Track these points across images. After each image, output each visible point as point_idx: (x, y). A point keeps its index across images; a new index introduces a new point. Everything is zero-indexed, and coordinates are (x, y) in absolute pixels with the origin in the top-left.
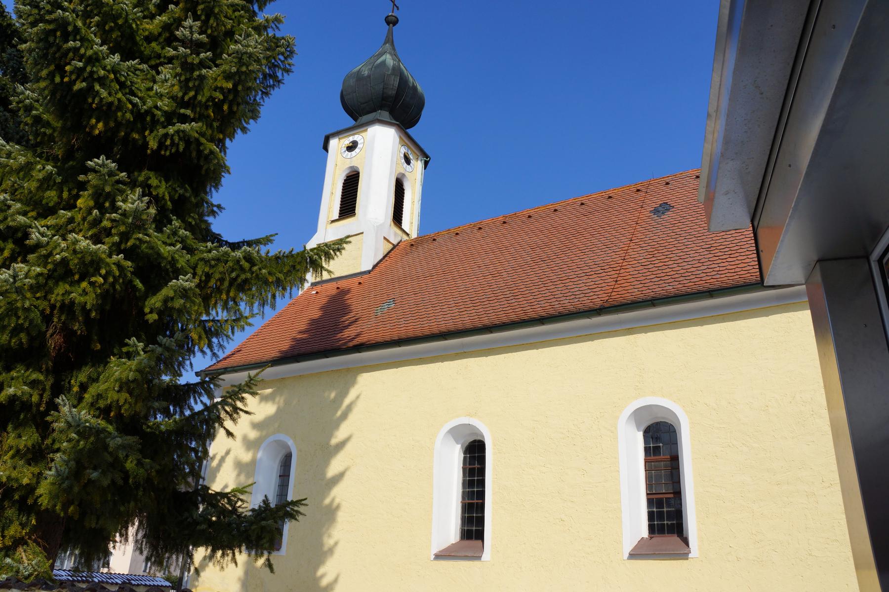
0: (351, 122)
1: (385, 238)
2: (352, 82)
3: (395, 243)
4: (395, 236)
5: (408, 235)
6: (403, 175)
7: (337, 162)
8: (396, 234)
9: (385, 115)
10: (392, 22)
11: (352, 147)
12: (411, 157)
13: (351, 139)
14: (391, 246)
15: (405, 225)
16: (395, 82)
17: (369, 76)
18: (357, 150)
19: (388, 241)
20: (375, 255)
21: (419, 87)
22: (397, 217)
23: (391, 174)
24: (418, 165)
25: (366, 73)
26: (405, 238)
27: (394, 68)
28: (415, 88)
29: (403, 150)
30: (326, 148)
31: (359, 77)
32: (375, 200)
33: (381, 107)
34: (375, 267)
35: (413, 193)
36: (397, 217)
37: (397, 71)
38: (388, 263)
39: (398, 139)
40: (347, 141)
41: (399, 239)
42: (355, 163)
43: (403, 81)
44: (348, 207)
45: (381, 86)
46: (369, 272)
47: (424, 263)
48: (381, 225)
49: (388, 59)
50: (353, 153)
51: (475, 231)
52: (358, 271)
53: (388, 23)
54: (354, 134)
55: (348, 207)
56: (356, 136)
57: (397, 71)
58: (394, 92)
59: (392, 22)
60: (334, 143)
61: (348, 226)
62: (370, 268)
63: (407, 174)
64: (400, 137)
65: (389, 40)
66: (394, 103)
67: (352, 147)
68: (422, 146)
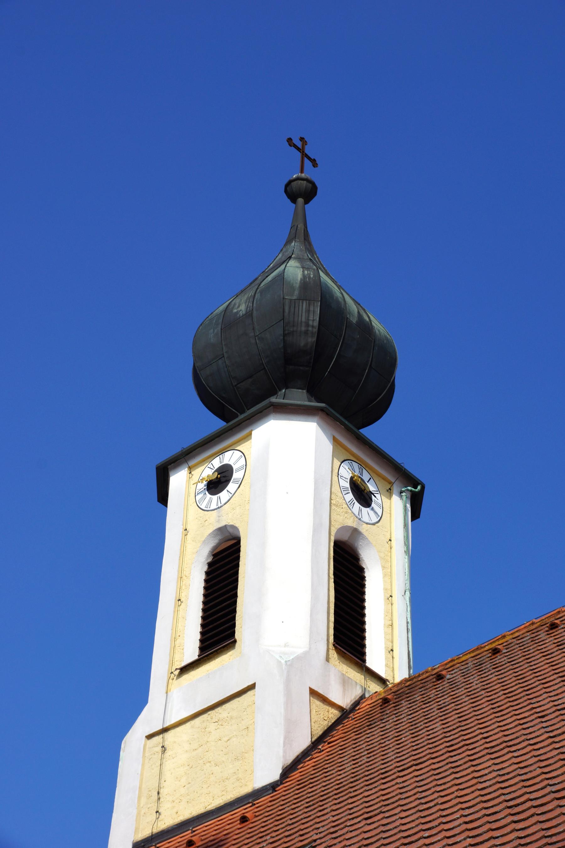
0: (218, 424)
1: (313, 693)
2: (213, 335)
3: (345, 702)
4: (344, 686)
5: (382, 681)
6: (355, 532)
7: (190, 518)
8: (345, 682)
9: (298, 396)
10: (301, 193)
11: (216, 485)
12: (371, 487)
13: (217, 463)
14: (334, 714)
15: (375, 658)
16: (310, 316)
17: (249, 314)
18: (232, 487)
19: (325, 700)
20: (288, 740)
21: (377, 325)
22: (349, 634)
23: (316, 529)
24: (393, 508)
25: (241, 307)
26: (374, 687)
27: (305, 285)
28: (365, 328)
29: (346, 472)
30: (163, 498)
31: (229, 323)
32: (285, 602)
33: (286, 382)
34: (287, 772)
35: (388, 575)
36: (349, 634)
37: (313, 290)
38: (323, 755)
39: (328, 446)
40: (207, 471)
41: (356, 693)
42: (228, 518)
43: (332, 311)
44: (218, 631)
45: (280, 331)
46: (273, 787)
47: (406, 737)
48: (298, 658)
49: (294, 271)
50: (224, 495)
51: (543, 635)
52: (247, 789)
53: (292, 196)
54: (222, 452)
55: (218, 631)
56: (228, 454)
57: (313, 290)
58: (312, 340)
59: (301, 193)
60: (178, 480)
61: (224, 672)
62: (275, 776)
63: (364, 529)
64: (335, 441)
65: (301, 233)
66: (336, 374)
67: (216, 485)
68: (398, 458)
